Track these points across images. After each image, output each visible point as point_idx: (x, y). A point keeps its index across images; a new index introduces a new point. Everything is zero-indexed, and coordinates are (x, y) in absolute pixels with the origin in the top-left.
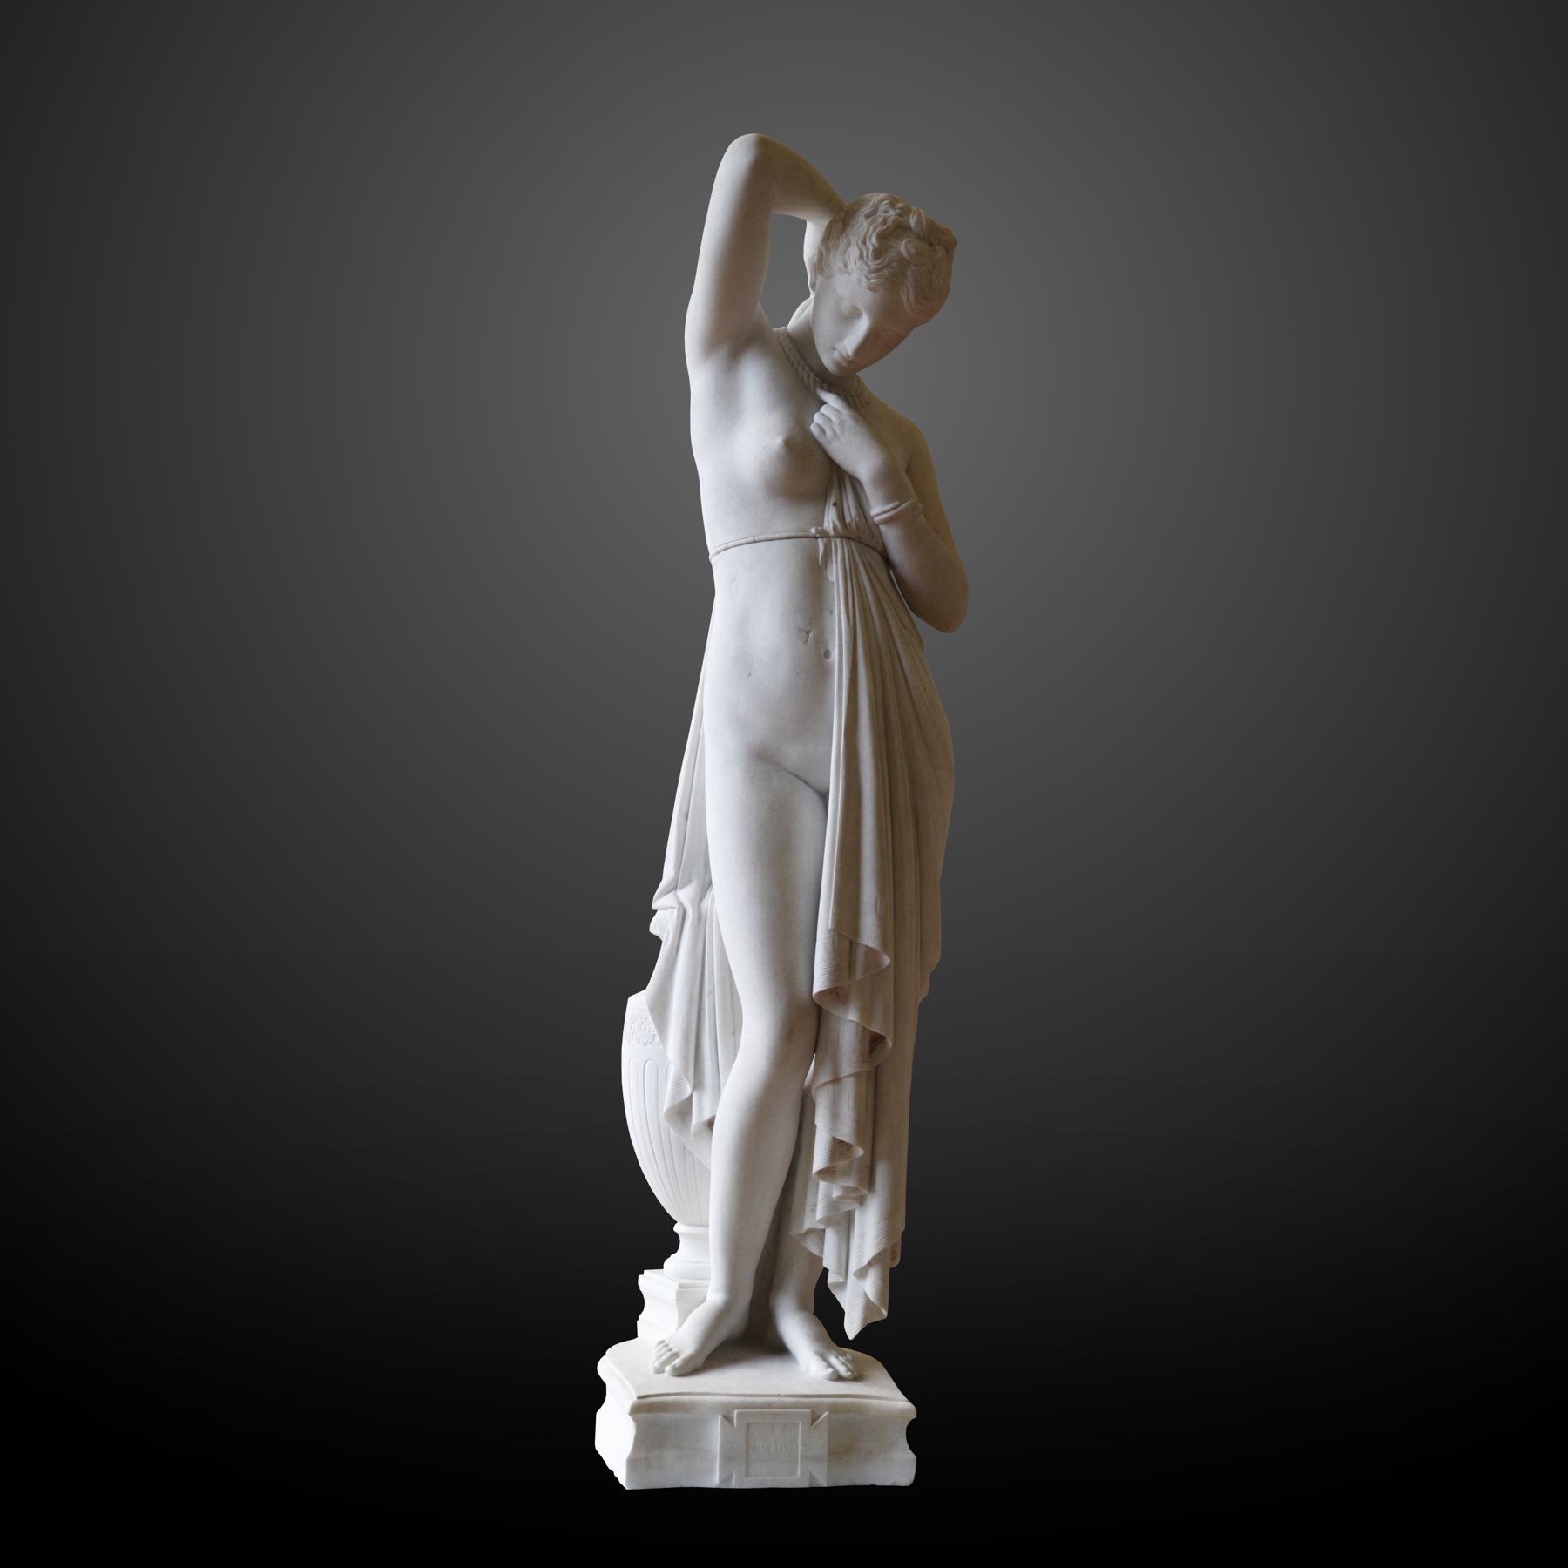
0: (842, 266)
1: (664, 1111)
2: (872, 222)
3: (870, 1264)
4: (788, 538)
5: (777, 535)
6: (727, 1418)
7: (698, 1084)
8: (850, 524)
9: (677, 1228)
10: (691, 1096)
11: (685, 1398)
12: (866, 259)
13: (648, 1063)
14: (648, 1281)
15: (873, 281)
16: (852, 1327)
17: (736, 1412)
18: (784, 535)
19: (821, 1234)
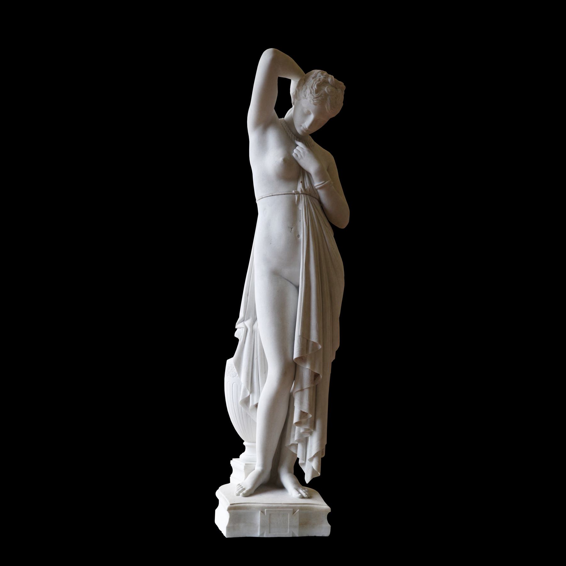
0: (304, 96)
1: (240, 401)
2: (315, 80)
3: (314, 456)
4: (284, 194)
5: (280, 193)
6: (263, 512)
7: (252, 391)
8: (307, 189)
9: (244, 443)
10: (249, 396)
11: (247, 505)
12: (312, 94)
13: (234, 384)
14: (234, 462)
15: (315, 101)
16: (308, 479)
17: (266, 510)
18: (283, 193)
19: (296, 445)
